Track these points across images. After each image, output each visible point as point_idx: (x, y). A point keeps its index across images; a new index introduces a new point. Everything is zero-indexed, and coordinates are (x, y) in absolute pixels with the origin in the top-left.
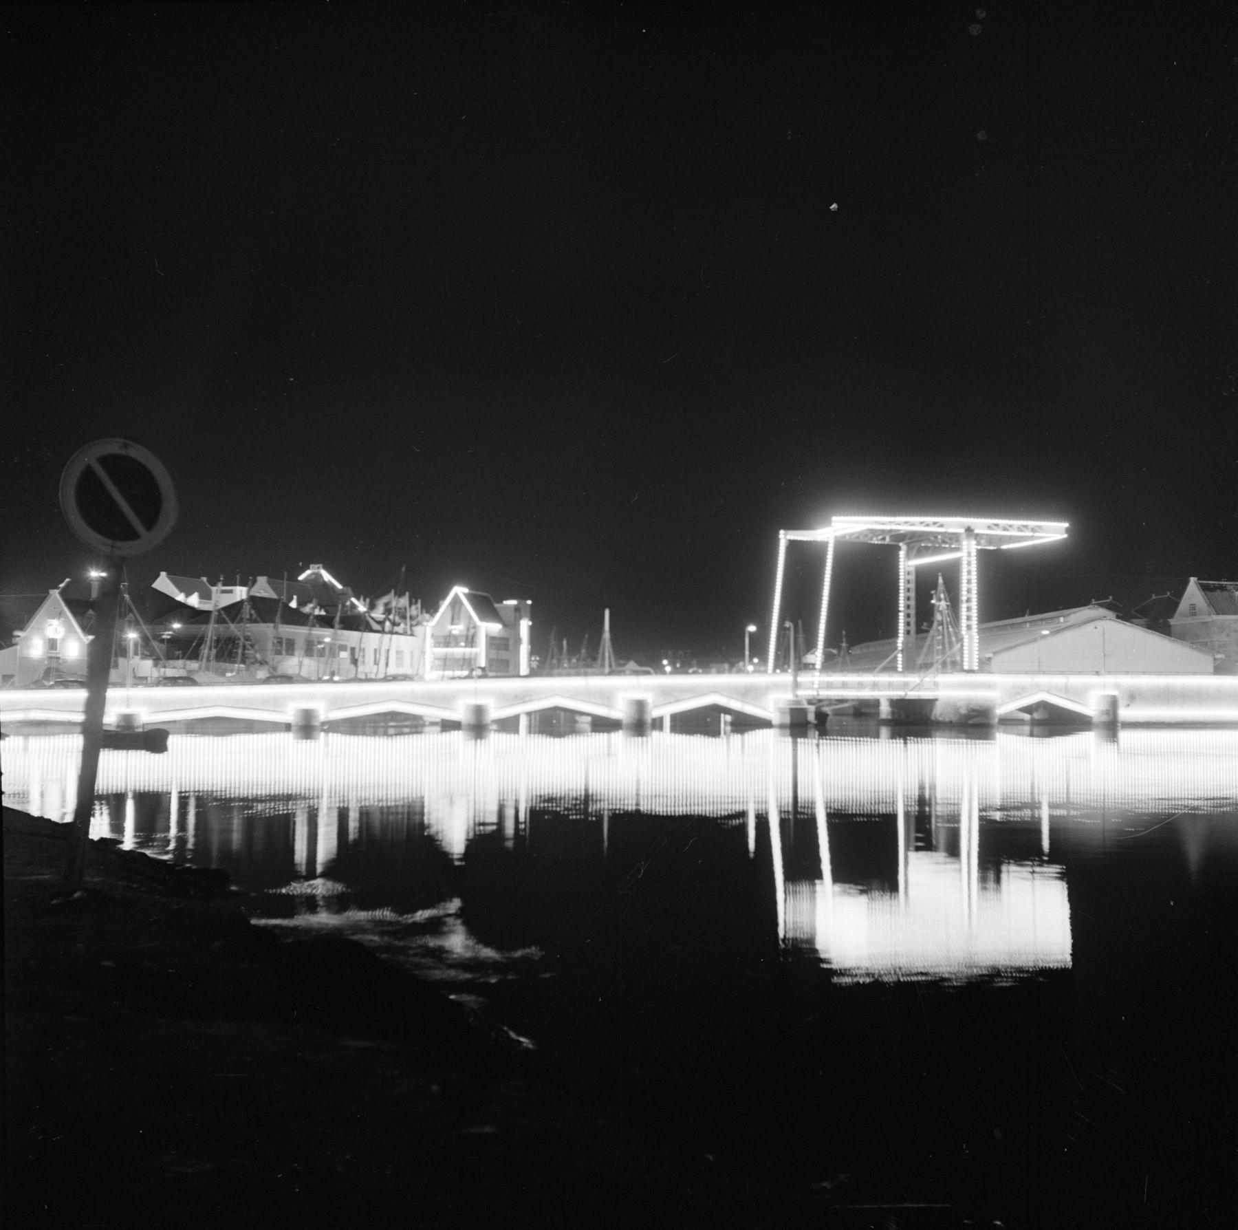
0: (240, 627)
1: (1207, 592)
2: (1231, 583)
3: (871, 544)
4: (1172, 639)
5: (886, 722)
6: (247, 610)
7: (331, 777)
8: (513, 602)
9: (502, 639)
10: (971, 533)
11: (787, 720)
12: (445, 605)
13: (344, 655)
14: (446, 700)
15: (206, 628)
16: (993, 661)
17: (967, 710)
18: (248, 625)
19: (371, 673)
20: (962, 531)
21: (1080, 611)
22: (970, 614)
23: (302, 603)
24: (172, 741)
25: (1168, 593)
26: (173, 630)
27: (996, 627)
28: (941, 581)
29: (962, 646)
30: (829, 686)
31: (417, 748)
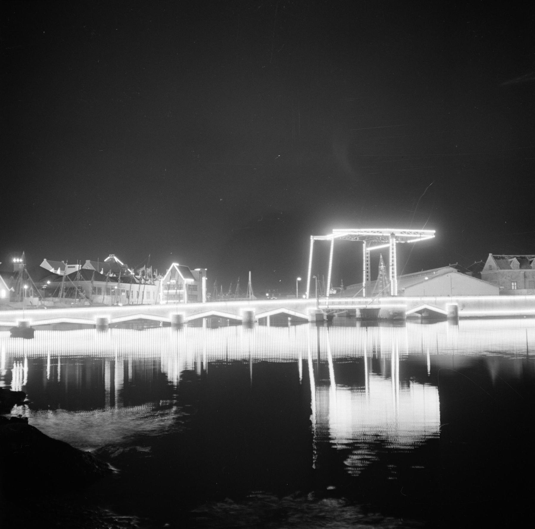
0: (76, 283)
1: (497, 260)
2: (507, 256)
3: (351, 241)
4: (481, 280)
5: (358, 319)
6: (79, 275)
7: (176, 346)
8: (199, 270)
9: (193, 286)
10: (394, 235)
11: (315, 319)
12: (169, 271)
13: (124, 294)
14: (163, 313)
15: (61, 283)
16: (405, 291)
17: (393, 313)
18: (79, 282)
19: (135, 302)
20: (389, 235)
21: (440, 270)
22: (393, 271)
23: (106, 272)
24: (36, 333)
25: (482, 261)
26: (48, 285)
27: (407, 276)
28: (381, 257)
29: (390, 285)
30: (333, 303)
31: (79, 338)
